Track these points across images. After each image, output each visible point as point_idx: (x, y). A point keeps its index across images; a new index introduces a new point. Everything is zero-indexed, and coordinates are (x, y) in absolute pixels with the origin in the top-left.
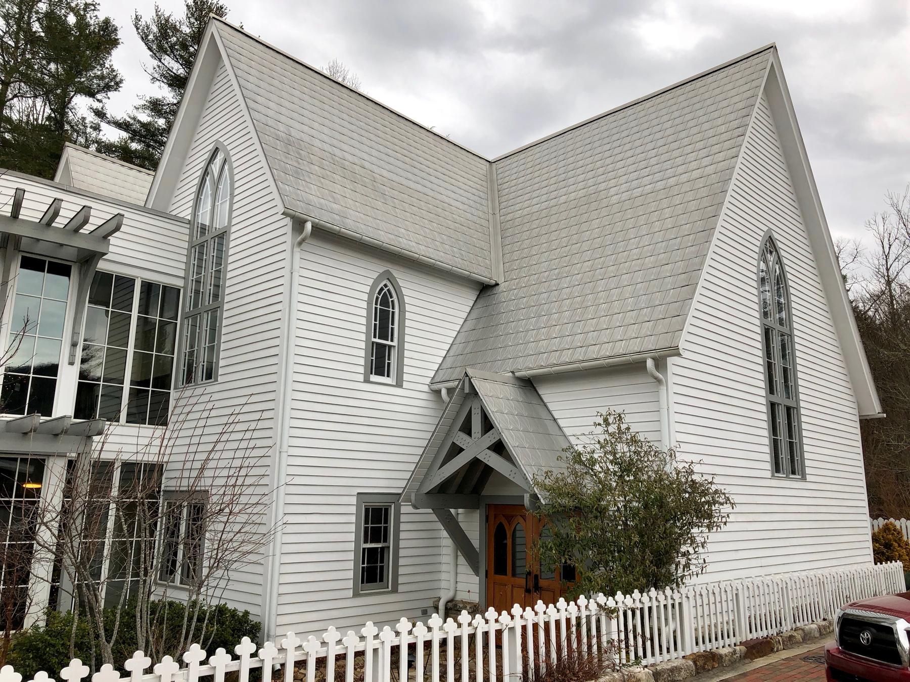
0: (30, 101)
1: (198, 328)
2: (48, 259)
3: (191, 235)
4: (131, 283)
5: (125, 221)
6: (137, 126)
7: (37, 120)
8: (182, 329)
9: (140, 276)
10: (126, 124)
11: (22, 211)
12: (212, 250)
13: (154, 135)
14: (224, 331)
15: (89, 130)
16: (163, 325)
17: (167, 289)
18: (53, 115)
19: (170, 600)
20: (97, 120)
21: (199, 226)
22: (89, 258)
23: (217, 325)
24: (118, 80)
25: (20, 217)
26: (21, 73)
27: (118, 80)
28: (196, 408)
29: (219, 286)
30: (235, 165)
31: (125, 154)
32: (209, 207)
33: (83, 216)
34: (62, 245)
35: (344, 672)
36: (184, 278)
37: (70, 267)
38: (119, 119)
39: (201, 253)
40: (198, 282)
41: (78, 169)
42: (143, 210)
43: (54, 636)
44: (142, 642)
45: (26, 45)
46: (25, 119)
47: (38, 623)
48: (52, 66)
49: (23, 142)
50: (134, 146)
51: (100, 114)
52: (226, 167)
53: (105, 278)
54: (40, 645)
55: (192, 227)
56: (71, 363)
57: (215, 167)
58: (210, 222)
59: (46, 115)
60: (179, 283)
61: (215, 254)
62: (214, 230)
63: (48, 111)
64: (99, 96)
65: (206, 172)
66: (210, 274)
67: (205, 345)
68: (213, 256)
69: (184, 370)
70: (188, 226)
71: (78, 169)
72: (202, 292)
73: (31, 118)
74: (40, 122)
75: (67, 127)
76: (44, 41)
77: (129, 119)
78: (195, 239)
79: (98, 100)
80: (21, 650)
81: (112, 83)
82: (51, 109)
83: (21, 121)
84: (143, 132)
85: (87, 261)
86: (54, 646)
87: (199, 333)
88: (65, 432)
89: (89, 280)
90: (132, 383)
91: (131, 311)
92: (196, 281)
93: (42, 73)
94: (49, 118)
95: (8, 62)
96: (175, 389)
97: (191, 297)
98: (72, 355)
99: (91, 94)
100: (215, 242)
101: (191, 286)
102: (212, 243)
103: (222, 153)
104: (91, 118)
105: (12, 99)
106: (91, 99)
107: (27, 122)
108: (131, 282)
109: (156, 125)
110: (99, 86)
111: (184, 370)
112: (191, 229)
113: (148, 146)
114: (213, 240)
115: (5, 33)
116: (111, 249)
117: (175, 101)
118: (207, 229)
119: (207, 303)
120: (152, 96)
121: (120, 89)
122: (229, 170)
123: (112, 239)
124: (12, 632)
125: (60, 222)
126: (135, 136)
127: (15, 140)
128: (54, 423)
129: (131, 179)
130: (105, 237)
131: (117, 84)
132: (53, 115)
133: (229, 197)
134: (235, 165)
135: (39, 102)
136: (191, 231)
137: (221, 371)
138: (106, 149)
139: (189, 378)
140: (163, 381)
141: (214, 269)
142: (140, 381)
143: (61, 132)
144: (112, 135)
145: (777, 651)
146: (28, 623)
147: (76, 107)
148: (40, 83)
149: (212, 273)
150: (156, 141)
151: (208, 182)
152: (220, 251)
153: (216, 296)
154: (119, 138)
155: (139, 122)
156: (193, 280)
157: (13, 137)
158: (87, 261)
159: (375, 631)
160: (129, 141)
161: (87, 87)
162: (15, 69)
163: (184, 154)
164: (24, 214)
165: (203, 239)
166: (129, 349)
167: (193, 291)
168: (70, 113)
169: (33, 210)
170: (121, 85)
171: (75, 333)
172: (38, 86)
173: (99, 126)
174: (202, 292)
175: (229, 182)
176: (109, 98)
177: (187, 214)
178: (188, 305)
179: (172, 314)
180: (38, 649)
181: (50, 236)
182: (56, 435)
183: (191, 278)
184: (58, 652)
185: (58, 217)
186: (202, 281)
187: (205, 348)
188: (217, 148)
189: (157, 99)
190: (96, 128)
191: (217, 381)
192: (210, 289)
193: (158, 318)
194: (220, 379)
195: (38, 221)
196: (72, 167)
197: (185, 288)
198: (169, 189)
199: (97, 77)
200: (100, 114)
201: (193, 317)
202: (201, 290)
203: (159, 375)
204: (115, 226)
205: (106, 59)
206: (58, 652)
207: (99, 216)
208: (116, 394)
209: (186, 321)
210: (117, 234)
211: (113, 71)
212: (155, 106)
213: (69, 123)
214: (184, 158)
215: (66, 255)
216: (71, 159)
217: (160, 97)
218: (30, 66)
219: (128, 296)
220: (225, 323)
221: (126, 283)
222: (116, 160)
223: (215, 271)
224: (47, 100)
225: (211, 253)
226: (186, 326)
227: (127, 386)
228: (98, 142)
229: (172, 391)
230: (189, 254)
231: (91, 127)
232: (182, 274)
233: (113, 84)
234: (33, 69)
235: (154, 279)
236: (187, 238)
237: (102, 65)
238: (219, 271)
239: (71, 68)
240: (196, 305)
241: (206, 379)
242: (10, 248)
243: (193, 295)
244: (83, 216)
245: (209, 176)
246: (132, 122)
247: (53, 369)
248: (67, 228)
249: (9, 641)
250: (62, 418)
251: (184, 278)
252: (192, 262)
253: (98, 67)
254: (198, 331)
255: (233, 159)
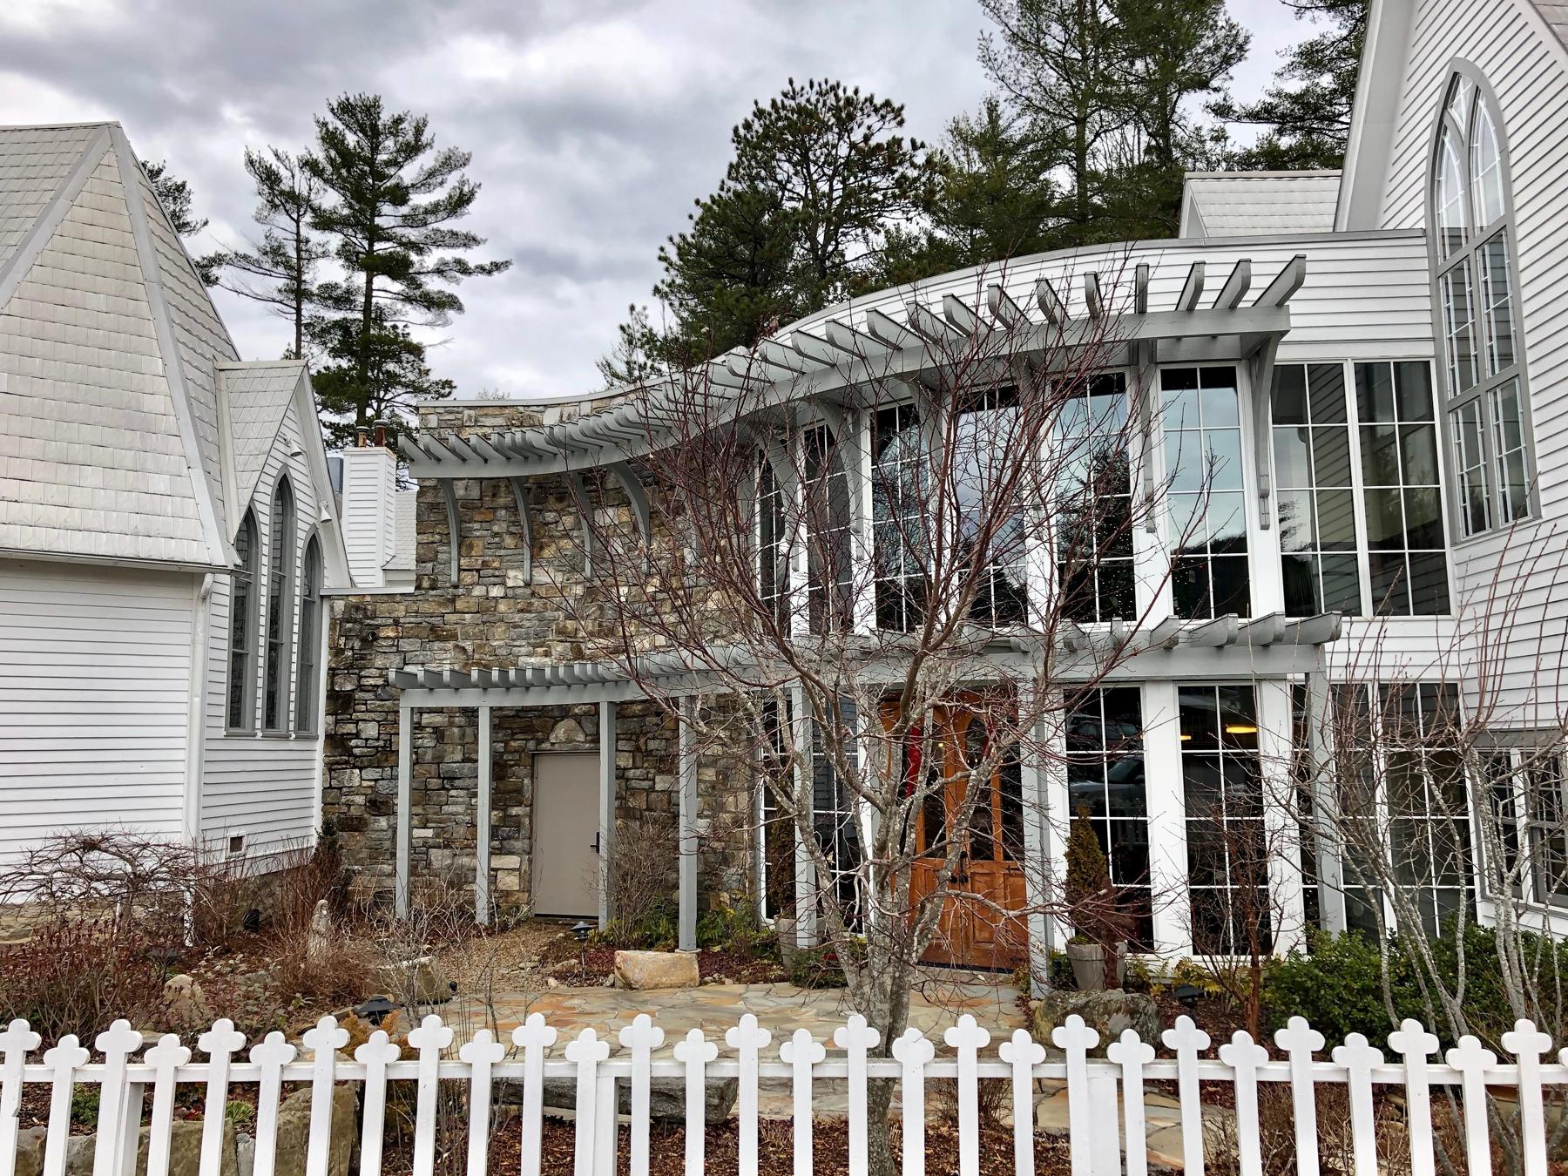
0: (1117, 133)
1: (1478, 425)
2: (1198, 366)
3: (1432, 257)
4: (1336, 372)
5: (1309, 268)
6: (1285, 107)
7: (1132, 160)
8: (1447, 432)
9: (1349, 357)
10: (1266, 110)
11: (1150, 300)
12: (1481, 272)
13: (1317, 108)
14: (1536, 419)
15: (1209, 145)
16: (1406, 432)
17: (1403, 367)
18: (1153, 143)
19: (1522, 929)
20: (1218, 123)
21: (1446, 234)
22: (1259, 347)
23: (1520, 410)
24: (1240, 40)
25: (1149, 310)
26: (1101, 97)
27: (1240, 40)
28: (1543, 564)
29: (1509, 337)
30: (1499, 91)
31: (1272, 159)
32: (1461, 192)
33: (1240, 280)
34: (1214, 337)
35: (1519, 1114)
36: (1433, 339)
37: (1234, 368)
38: (1253, 105)
39: (1459, 284)
40: (1463, 339)
41: (1212, 209)
42: (1334, 237)
43: (1328, 971)
44: (1517, 1001)
45: (1097, 47)
46: (1115, 165)
47: (1298, 947)
48: (1139, 65)
49: (1120, 200)
50: (1286, 142)
51: (1223, 111)
52: (1481, 103)
53: (1290, 376)
54: (1309, 984)
55: (1431, 241)
56: (1265, 527)
57: (1459, 112)
58: (1467, 221)
59: (1143, 146)
60: (1425, 350)
61: (1489, 277)
62: (1477, 232)
63: (1145, 138)
64: (1215, 83)
65: (1441, 129)
66: (1484, 319)
67: (1501, 453)
68: (1486, 282)
69: (1465, 508)
70: (1423, 241)
71: (1212, 209)
72: (1476, 356)
73: (1124, 161)
74: (1136, 162)
75: (1176, 153)
76: (1120, 31)
77: (1269, 100)
78: (1440, 260)
79: (1216, 90)
80: (1278, 988)
81: (1233, 50)
82: (1149, 134)
83: (1110, 170)
84: (1298, 111)
85: (1258, 353)
86: (1331, 987)
87: (1482, 433)
88: (1278, 639)
89: (1267, 383)
90: (1371, 545)
91: (1345, 420)
92: (1458, 339)
93: (1127, 83)
94: (1148, 150)
95: (1078, 87)
96: (1453, 544)
97: (1453, 370)
98: (1264, 513)
99: (1203, 84)
100: (1484, 255)
101: (1449, 351)
102: (1479, 258)
103: (1468, 78)
104: (1209, 122)
105: (1094, 141)
106: (1205, 92)
107: (1119, 170)
108: (1336, 370)
109: (1318, 90)
110: (1213, 64)
111: (1465, 508)
112: (1431, 246)
113: (1310, 131)
114: (1479, 252)
115: (1065, 44)
116: (1294, 321)
117: (1345, 33)
118: (1463, 234)
119: (1489, 374)
120: (1301, 42)
121: (1247, 55)
122: (1487, 106)
123: (1293, 306)
124: (1260, 957)
125: (1207, 300)
126: (1284, 124)
127: (1108, 203)
128: (1259, 625)
129: (1297, 196)
130: (1280, 304)
131: (1241, 48)
132: (1153, 143)
133: (1498, 159)
134: (1499, 91)
135: (1130, 130)
136: (1432, 248)
137: (1544, 498)
138: (1247, 162)
139: (1479, 522)
140: (1428, 533)
141: (1492, 306)
142: (1385, 540)
143: (1169, 165)
144: (1246, 137)
145: (1379, 1165)
146: (1281, 950)
147: (1185, 114)
148: (1129, 98)
149: (1488, 314)
150: (1321, 119)
151: (1448, 145)
152: (1499, 268)
153: (1506, 358)
154: (1258, 139)
155: (1288, 96)
156: (1451, 339)
157: (1104, 200)
158: (1258, 353)
159: (238, 1041)
160: (1276, 137)
161: (1196, 74)
162: (1090, 94)
163: (1389, 114)
164: (1154, 303)
165: (1460, 255)
166: (1354, 487)
167: (1456, 359)
168: (1178, 130)
169: (1164, 295)
170: (1247, 47)
171: (1261, 476)
172: (1126, 106)
173: (1223, 130)
174: (1476, 356)
175: (1492, 129)
176: (1231, 78)
177: (1416, 219)
178: (1449, 386)
179: (1423, 411)
180: (1307, 990)
181: (1197, 327)
182: (1266, 646)
183: (1446, 335)
184: (1340, 999)
185: (1203, 294)
186: (1471, 335)
187: (1501, 459)
188: (1456, 74)
189: (1311, 44)
190: (1220, 137)
191: (1540, 517)
192: (1491, 347)
193: (1396, 423)
194: (1546, 513)
195: (1173, 308)
196: (1201, 210)
197: (1438, 358)
198: (1373, 192)
199: (1208, 51)
200: (1223, 111)
201: (1467, 411)
202: (1473, 353)
203: (1418, 524)
204: (1293, 279)
205: (1217, 14)
206: (1340, 999)
207: (1265, 268)
208: (1346, 569)
209: (1452, 417)
210: (1298, 294)
211: (1232, 27)
212: (1312, 58)
213: (1178, 146)
214: (1392, 120)
215: (1225, 350)
216: (1198, 198)
217: (1317, 38)
218: (1108, 80)
219: (1337, 395)
220: (1535, 403)
221: (1329, 374)
222: (1266, 173)
223: (1495, 309)
224: (1139, 121)
225: (1479, 277)
226: (1453, 427)
227: (1363, 553)
228: (1229, 158)
229: (1448, 549)
230: (1434, 293)
231: (1212, 139)
232: (1427, 332)
233: (1234, 50)
234: (1114, 83)
235: (1377, 355)
236: (1425, 264)
237: (1214, 27)
238: (1504, 308)
239: (1165, 54)
240: (1466, 384)
241: (1474, 532)
242: (1144, 361)
243: (1456, 365)
244: (1240, 280)
245: (1448, 133)
246: (1275, 101)
247: (1240, 543)
248: (1217, 306)
249: (1258, 972)
250: (1269, 617)
251: (1433, 339)
252: (1444, 305)
253: (1208, 33)
254: (1479, 430)
255: (1494, 81)
